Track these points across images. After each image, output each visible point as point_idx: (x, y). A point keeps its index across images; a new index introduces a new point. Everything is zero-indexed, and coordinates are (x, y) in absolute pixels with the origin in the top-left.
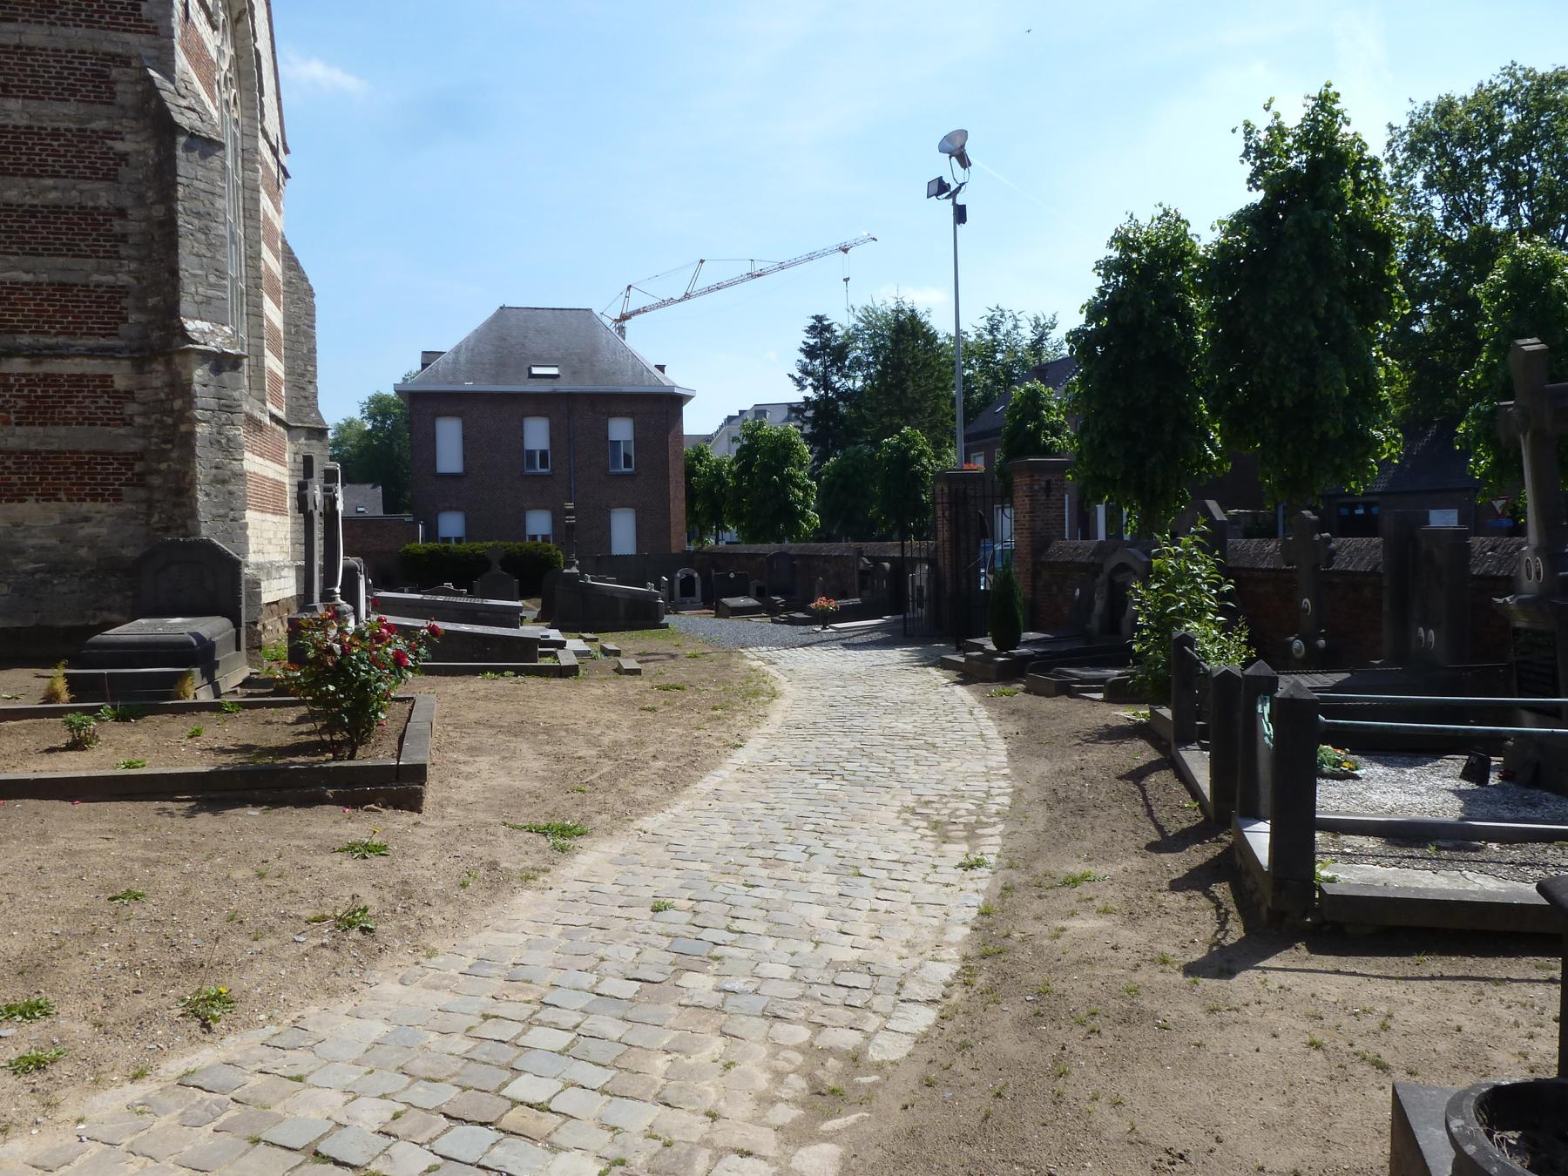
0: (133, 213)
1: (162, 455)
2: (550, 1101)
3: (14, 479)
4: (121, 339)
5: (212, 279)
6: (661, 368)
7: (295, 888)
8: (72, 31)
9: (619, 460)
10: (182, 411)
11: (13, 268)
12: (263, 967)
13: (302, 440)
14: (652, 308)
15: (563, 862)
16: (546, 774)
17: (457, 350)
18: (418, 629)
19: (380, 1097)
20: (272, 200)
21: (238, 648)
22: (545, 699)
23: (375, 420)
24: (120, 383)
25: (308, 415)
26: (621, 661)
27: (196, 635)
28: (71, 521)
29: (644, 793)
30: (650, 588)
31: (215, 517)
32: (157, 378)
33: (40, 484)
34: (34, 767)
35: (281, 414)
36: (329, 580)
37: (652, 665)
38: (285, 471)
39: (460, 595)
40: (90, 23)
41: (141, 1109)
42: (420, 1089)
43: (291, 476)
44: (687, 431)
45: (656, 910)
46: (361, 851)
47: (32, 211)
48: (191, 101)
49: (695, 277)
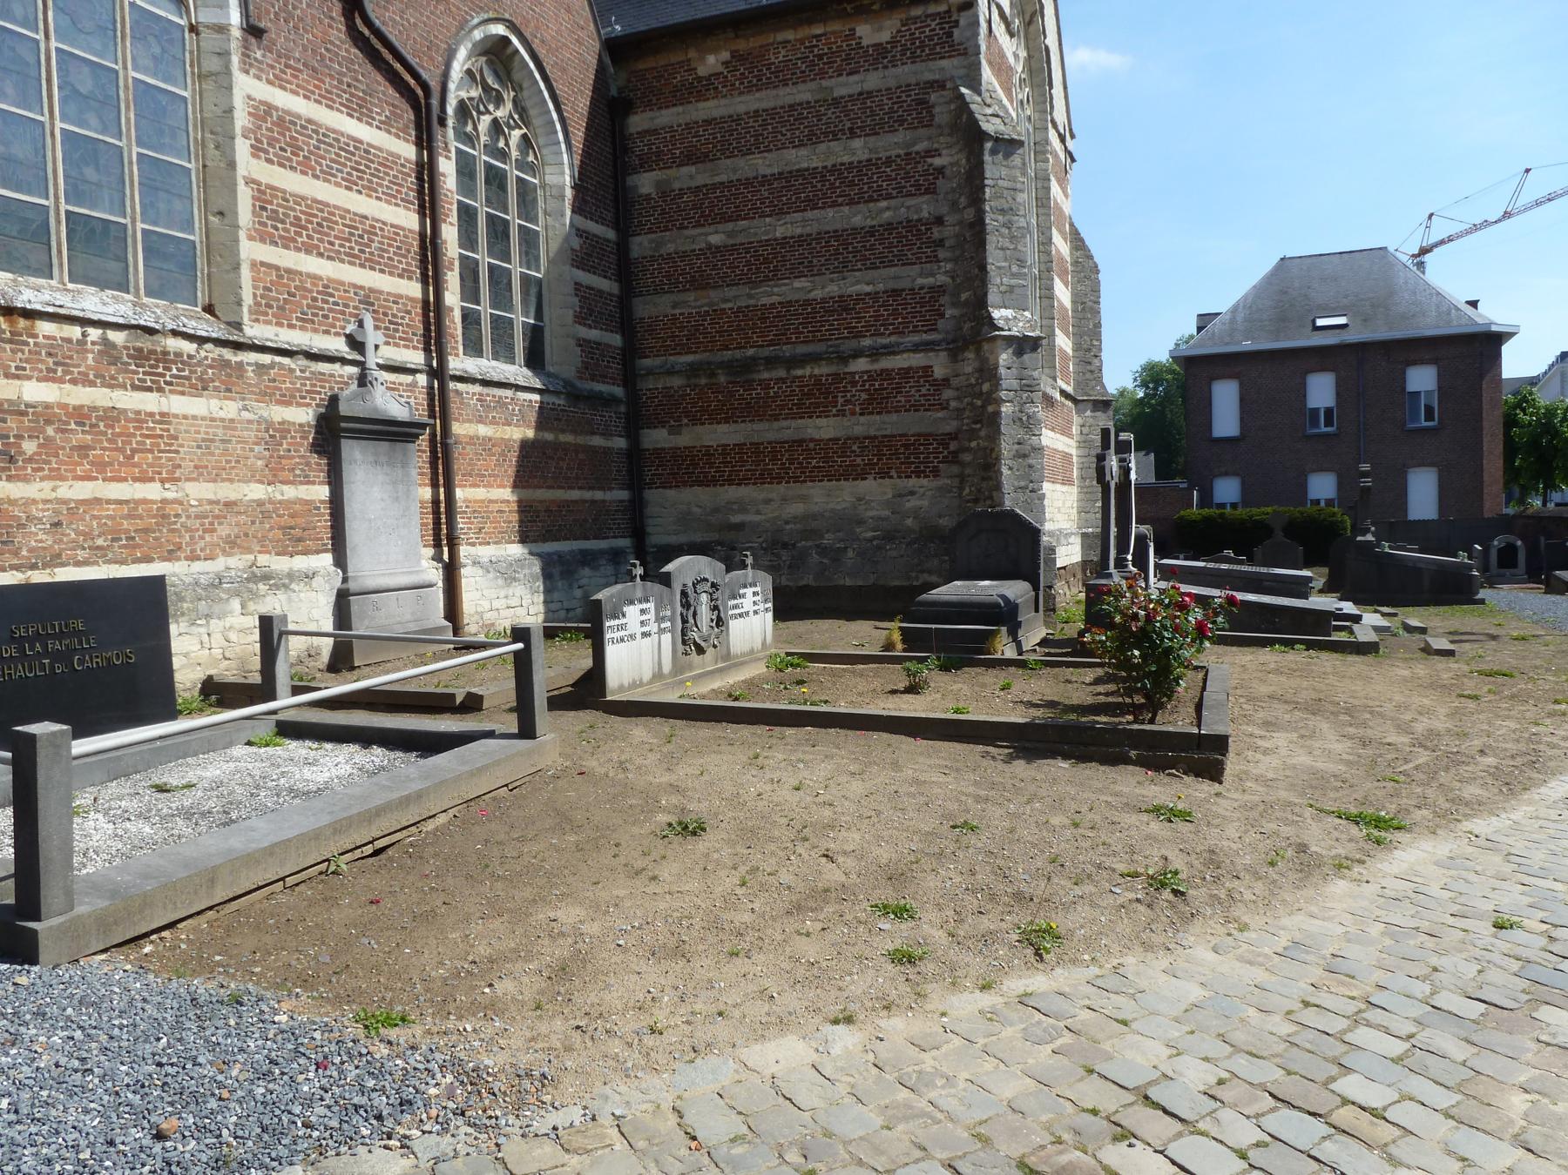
0: (949, 219)
1: (973, 435)
2: (1385, 1109)
3: (859, 460)
4: (939, 333)
5: (1015, 269)
6: (1474, 304)
7: (1108, 841)
8: (899, 70)
9: (1419, 414)
10: (990, 393)
11: (858, 282)
12: (1084, 911)
13: (1088, 413)
14: (1460, 235)
15: (1379, 855)
16: (1351, 758)
17: (1234, 310)
18: (1214, 597)
19: (1203, 1059)
20: (1060, 185)
21: (1037, 610)
22: (1344, 677)
23: (1148, 387)
24: (939, 372)
25: (1093, 388)
26: (1429, 639)
27: (1003, 597)
28: (900, 496)
29: (1472, 791)
30: (1463, 558)
31: (1017, 489)
32: (969, 365)
33: (877, 464)
34: (882, 705)
35: (1069, 389)
36: (1122, 547)
37: (1467, 646)
38: (1073, 443)
39: (1241, 563)
40: (914, 59)
41: (990, 1016)
42: (1243, 1061)
43: (1078, 447)
44: (1505, 375)
45: (1499, 926)
46: (1170, 815)
47: (872, 232)
48: (995, 109)
49: (1518, 191)
